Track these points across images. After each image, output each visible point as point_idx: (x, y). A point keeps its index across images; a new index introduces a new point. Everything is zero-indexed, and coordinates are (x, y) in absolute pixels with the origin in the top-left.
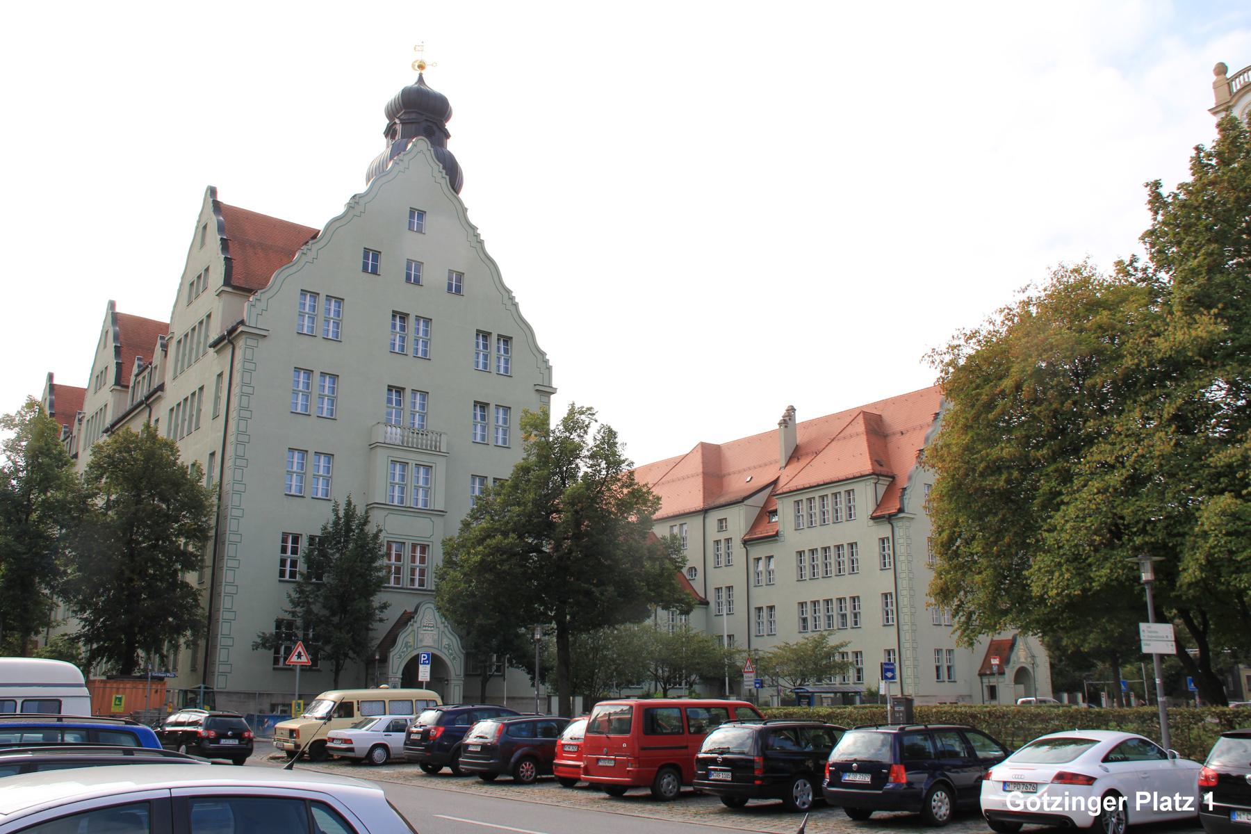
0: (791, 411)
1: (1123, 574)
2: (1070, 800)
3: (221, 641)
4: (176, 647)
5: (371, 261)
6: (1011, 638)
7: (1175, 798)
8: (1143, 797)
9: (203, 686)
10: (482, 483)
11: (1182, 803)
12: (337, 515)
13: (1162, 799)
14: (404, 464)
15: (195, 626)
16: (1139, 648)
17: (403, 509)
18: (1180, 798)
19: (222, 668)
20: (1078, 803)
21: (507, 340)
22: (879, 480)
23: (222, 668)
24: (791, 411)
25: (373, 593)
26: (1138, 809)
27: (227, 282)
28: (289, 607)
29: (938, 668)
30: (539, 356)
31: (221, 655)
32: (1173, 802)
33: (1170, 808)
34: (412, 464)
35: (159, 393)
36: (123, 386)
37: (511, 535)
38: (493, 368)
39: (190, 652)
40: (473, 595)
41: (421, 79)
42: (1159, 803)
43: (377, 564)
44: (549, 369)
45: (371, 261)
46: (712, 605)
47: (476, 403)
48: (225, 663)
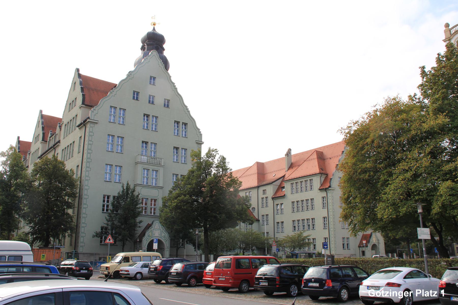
0: (290, 150)
1: (411, 210)
2: (392, 292)
3: (81, 234)
4: (64, 237)
5: (136, 96)
6: (370, 233)
7: (430, 292)
8: (419, 292)
9: (74, 251)
10: (176, 177)
11: (433, 294)
12: (123, 188)
13: (426, 292)
14: (148, 170)
15: (71, 229)
16: (417, 237)
17: (148, 186)
18: (432, 292)
19: (81, 244)
20: (395, 294)
21: (186, 124)
22: (322, 175)
23: (81, 244)
24: (290, 150)
25: (136, 217)
26: (417, 296)
27: (83, 103)
28: (106, 222)
29: (343, 244)
30: (197, 130)
31: (81, 240)
32: (430, 293)
33: (428, 296)
34: (151, 170)
35: (58, 144)
36: (45, 141)
37: (187, 196)
38: (181, 135)
39: (69, 238)
40: (173, 218)
41: (154, 29)
42: (424, 293)
43: (138, 206)
44: (201, 135)
45: (136, 96)
46: (261, 221)
47: (174, 147)
48: (82, 242)
